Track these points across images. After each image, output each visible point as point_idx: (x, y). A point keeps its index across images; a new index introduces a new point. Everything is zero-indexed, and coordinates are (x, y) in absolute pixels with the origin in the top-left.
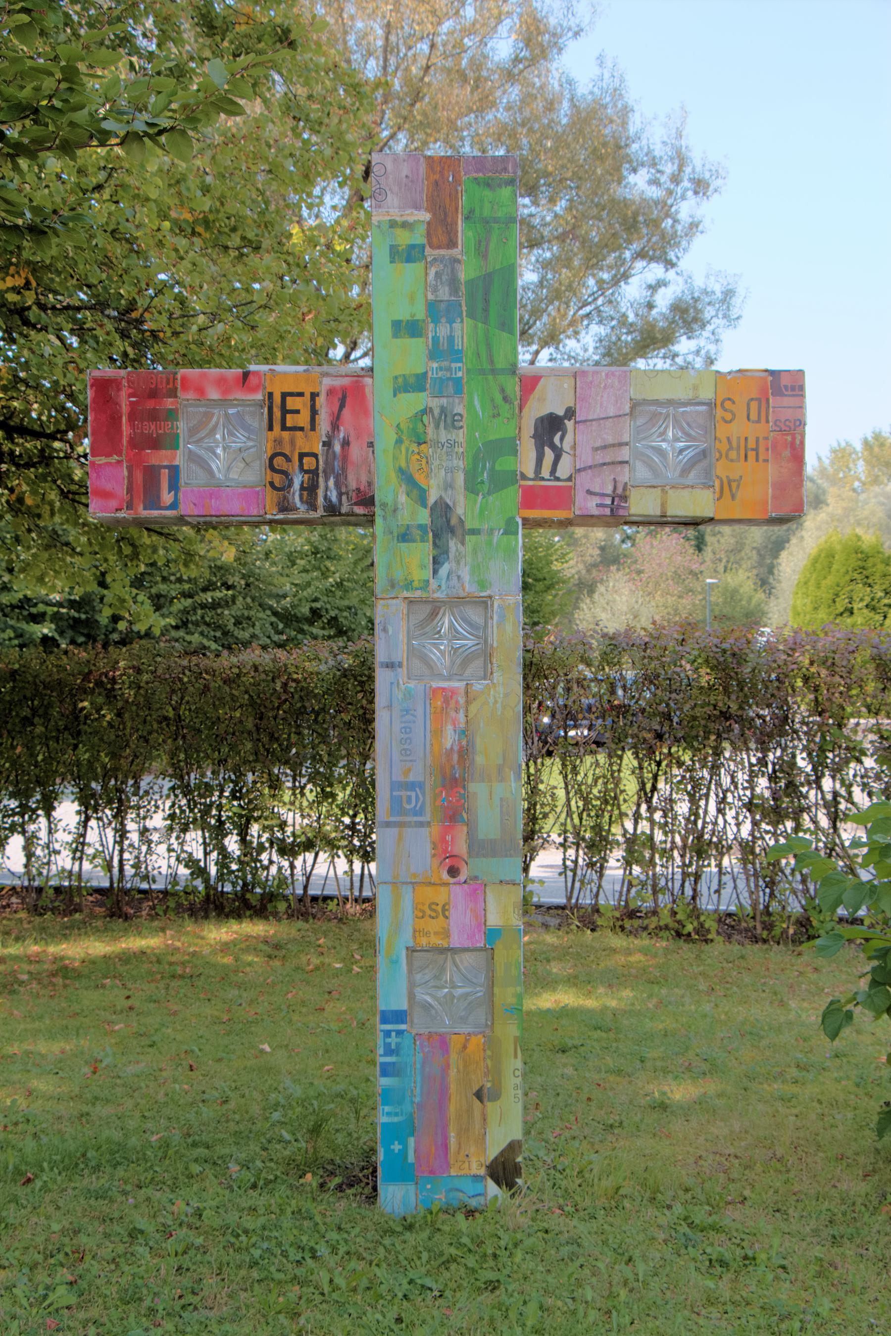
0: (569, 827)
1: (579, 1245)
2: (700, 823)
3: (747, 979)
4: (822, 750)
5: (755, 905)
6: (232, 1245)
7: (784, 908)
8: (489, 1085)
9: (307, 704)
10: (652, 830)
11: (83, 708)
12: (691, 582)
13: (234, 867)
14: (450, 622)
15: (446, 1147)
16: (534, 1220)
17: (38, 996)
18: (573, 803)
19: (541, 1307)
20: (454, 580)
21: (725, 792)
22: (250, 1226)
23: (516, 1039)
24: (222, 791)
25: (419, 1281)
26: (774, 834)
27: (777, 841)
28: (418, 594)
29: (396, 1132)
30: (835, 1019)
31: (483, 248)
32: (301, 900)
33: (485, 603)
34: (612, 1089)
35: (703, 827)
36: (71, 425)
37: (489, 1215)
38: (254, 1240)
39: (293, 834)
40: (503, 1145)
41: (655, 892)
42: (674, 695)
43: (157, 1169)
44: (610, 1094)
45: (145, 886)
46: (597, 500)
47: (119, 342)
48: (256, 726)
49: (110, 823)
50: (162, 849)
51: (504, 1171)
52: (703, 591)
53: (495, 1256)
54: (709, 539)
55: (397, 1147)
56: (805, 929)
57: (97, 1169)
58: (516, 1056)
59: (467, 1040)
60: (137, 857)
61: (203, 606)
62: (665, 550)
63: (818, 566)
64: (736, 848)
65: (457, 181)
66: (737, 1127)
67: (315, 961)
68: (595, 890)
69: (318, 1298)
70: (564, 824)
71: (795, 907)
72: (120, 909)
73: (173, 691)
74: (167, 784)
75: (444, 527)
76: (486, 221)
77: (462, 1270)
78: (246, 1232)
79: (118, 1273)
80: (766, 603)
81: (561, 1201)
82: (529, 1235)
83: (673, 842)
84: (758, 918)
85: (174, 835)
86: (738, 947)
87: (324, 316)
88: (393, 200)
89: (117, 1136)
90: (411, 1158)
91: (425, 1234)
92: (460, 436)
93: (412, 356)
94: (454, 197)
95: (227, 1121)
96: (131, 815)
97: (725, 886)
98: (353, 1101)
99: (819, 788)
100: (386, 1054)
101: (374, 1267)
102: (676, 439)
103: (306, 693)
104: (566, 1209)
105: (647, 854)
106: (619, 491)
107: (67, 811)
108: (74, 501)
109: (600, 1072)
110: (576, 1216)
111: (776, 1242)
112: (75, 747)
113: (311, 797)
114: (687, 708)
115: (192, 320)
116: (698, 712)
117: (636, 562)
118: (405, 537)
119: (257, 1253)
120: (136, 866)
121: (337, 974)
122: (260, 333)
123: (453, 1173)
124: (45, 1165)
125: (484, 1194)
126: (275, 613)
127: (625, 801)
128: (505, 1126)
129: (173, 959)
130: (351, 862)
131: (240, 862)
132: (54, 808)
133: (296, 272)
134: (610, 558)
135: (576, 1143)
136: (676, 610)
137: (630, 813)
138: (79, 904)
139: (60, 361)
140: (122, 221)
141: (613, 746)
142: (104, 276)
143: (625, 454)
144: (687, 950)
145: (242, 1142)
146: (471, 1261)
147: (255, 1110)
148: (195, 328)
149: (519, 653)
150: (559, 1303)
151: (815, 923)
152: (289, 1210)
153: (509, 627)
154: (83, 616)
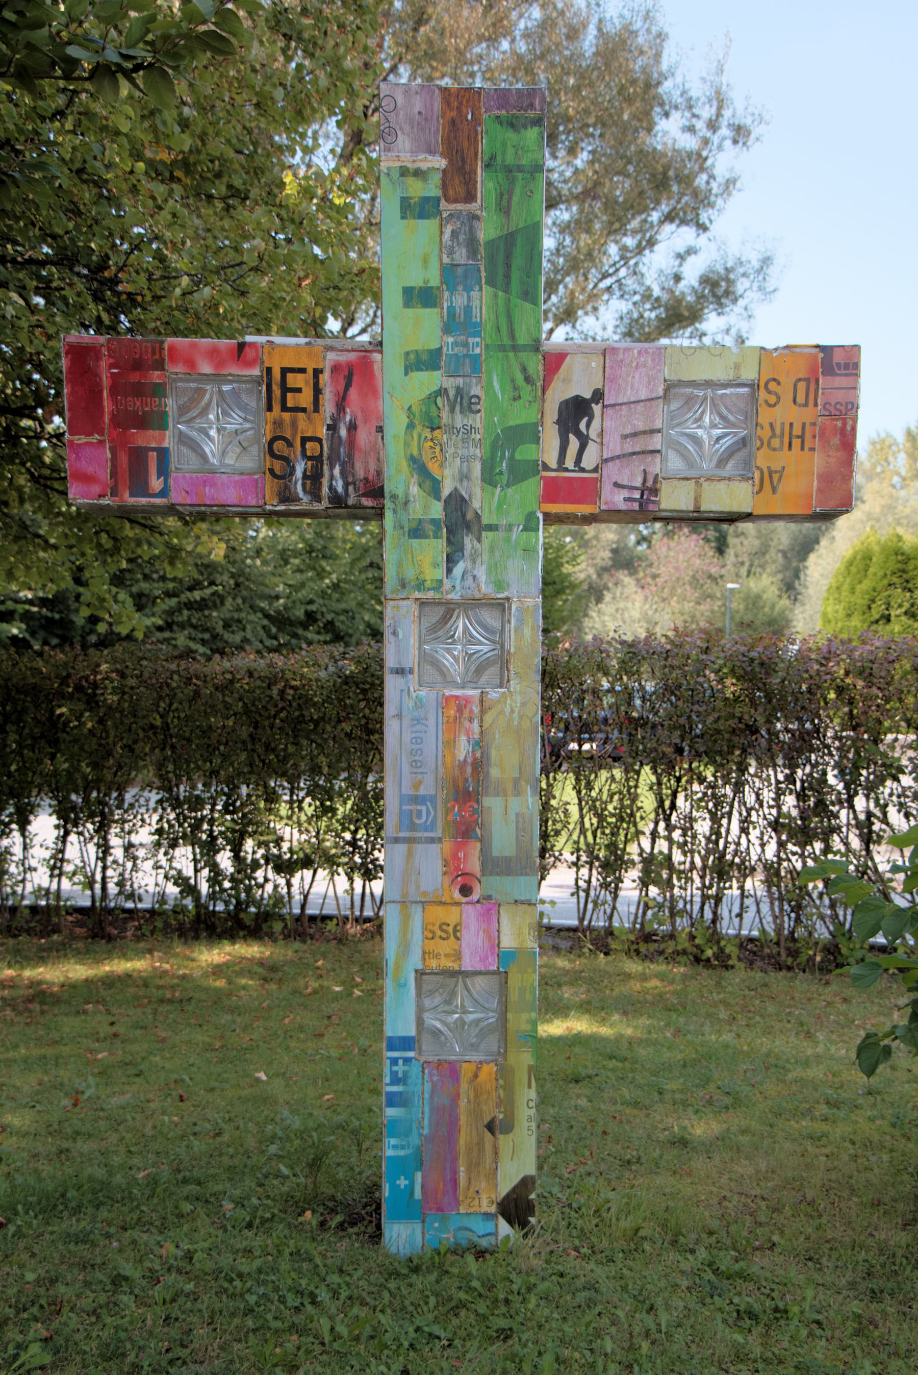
0: (582, 845)
1: (596, 1291)
2: (721, 842)
3: (771, 1009)
4: (856, 767)
5: (779, 930)
6: (226, 1290)
7: (810, 934)
8: (501, 1116)
9: (305, 713)
10: (670, 849)
11: (61, 715)
12: (708, 585)
13: (227, 885)
14: (465, 626)
15: (455, 1182)
16: (548, 1262)
17: (12, 1023)
18: (586, 820)
19: (557, 1359)
20: (469, 582)
21: (749, 811)
22: (245, 1269)
23: (530, 1068)
24: (214, 805)
25: (426, 1329)
26: (802, 856)
27: (804, 863)
28: (431, 595)
29: (402, 1166)
30: (871, 1054)
31: (504, 203)
32: (298, 919)
33: (501, 606)
34: (629, 1122)
35: (725, 847)
36: (41, 401)
37: (500, 1256)
38: (249, 1284)
39: (291, 850)
40: (516, 1181)
41: (673, 915)
42: (696, 707)
43: (144, 1208)
44: (627, 1127)
45: (130, 905)
46: (625, 494)
47: (92, 306)
48: (251, 736)
49: (92, 838)
50: (148, 865)
51: (516, 1208)
52: (724, 597)
53: (507, 1301)
54: (731, 540)
55: (403, 1182)
56: (833, 957)
57: (77, 1210)
58: (530, 1087)
59: (478, 1069)
60: (121, 875)
61: (189, 605)
62: (682, 552)
63: (853, 569)
64: (760, 868)
65: (477, 120)
66: (763, 1166)
67: (314, 984)
68: (609, 911)
69: (318, 1349)
70: (577, 842)
71: (822, 932)
72: (102, 929)
73: (161, 698)
74: (154, 797)
75: (459, 522)
76: (508, 170)
77: (472, 1316)
78: (240, 1276)
79: (100, 1325)
80: (792, 610)
81: (577, 1242)
82: (543, 1279)
83: (692, 863)
84: (782, 944)
85: (162, 850)
86: (760, 974)
87: (322, 281)
88: (404, 142)
89: (100, 1173)
90: (418, 1194)
91: (433, 1277)
92: (477, 421)
93: (424, 329)
94: (473, 139)
95: (221, 1155)
96: (115, 829)
97: (747, 908)
98: (355, 1132)
99: (851, 807)
100: (392, 1083)
101: (378, 1314)
102: (713, 426)
103: (305, 701)
104: (583, 1251)
105: (665, 874)
106: (650, 483)
107: (44, 825)
108: (46, 486)
109: (615, 1103)
110: (593, 1259)
111: (809, 1293)
112: (53, 757)
113: (310, 811)
114: (710, 720)
115: (176, 282)
116: (721, 725)
117: (651, 565)
118: (417, 532)
119: (252, 1299)
120: (120, 884)
121: (337, 997)
122: (253, 299)
123: (462, 1211)
124: (20, 1207)
125: (496, 1234)
126: (267, 616)
127: (642, 818)
128: (518, 1160)
129: (162, 982)
130: (351, 880)
131: (232, 879)
132: (29, 823)
133: (291, 228)
134: (623, 561)
135: (592, 1180)
136: (693, 617)
137: (648, 833)
138: (58, 924)
139: (24, 324)
140: (89, 158)
141: (630, 760)
142: (71, 225)
143: (656, 442)
144: (706, 977)
145: (237, 1178)
146: (482, 1307)
147: (251, 1142)
148: (178, 291)
149: (538, 660)
150: (577, 1355)
151: (844, 951)
152: (287, 1251)
153: (527, 632)
154: (57, 616)
